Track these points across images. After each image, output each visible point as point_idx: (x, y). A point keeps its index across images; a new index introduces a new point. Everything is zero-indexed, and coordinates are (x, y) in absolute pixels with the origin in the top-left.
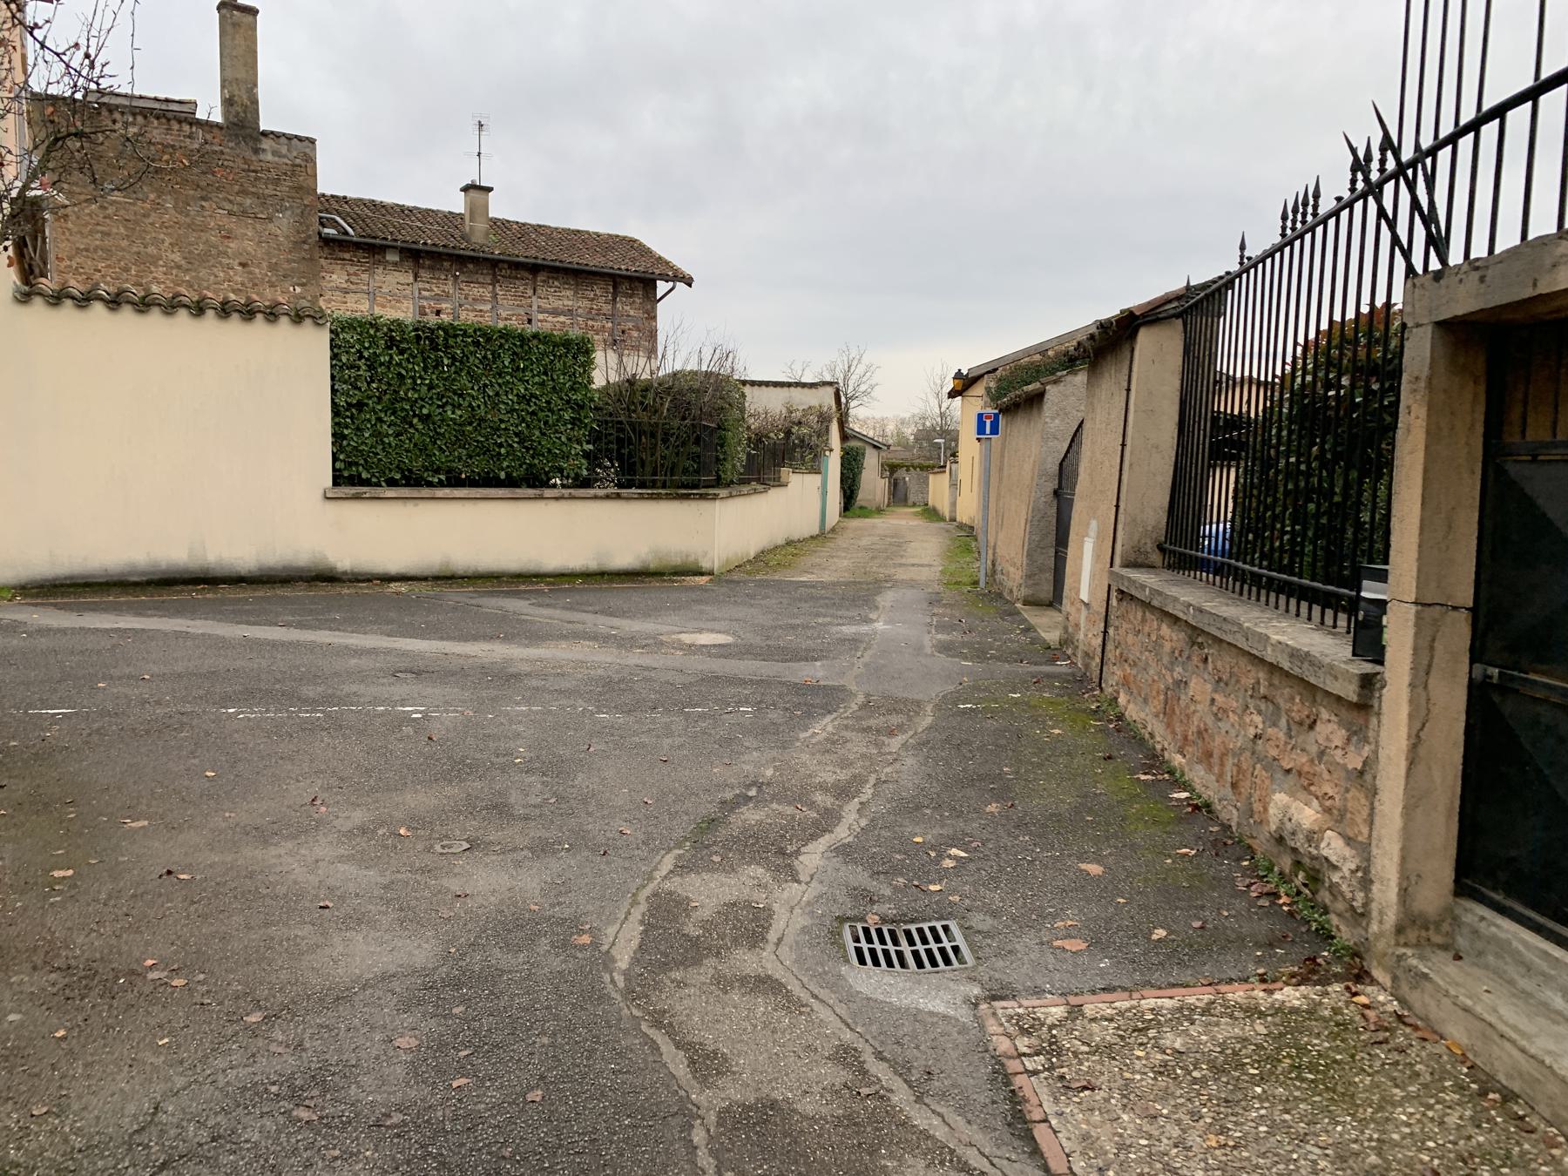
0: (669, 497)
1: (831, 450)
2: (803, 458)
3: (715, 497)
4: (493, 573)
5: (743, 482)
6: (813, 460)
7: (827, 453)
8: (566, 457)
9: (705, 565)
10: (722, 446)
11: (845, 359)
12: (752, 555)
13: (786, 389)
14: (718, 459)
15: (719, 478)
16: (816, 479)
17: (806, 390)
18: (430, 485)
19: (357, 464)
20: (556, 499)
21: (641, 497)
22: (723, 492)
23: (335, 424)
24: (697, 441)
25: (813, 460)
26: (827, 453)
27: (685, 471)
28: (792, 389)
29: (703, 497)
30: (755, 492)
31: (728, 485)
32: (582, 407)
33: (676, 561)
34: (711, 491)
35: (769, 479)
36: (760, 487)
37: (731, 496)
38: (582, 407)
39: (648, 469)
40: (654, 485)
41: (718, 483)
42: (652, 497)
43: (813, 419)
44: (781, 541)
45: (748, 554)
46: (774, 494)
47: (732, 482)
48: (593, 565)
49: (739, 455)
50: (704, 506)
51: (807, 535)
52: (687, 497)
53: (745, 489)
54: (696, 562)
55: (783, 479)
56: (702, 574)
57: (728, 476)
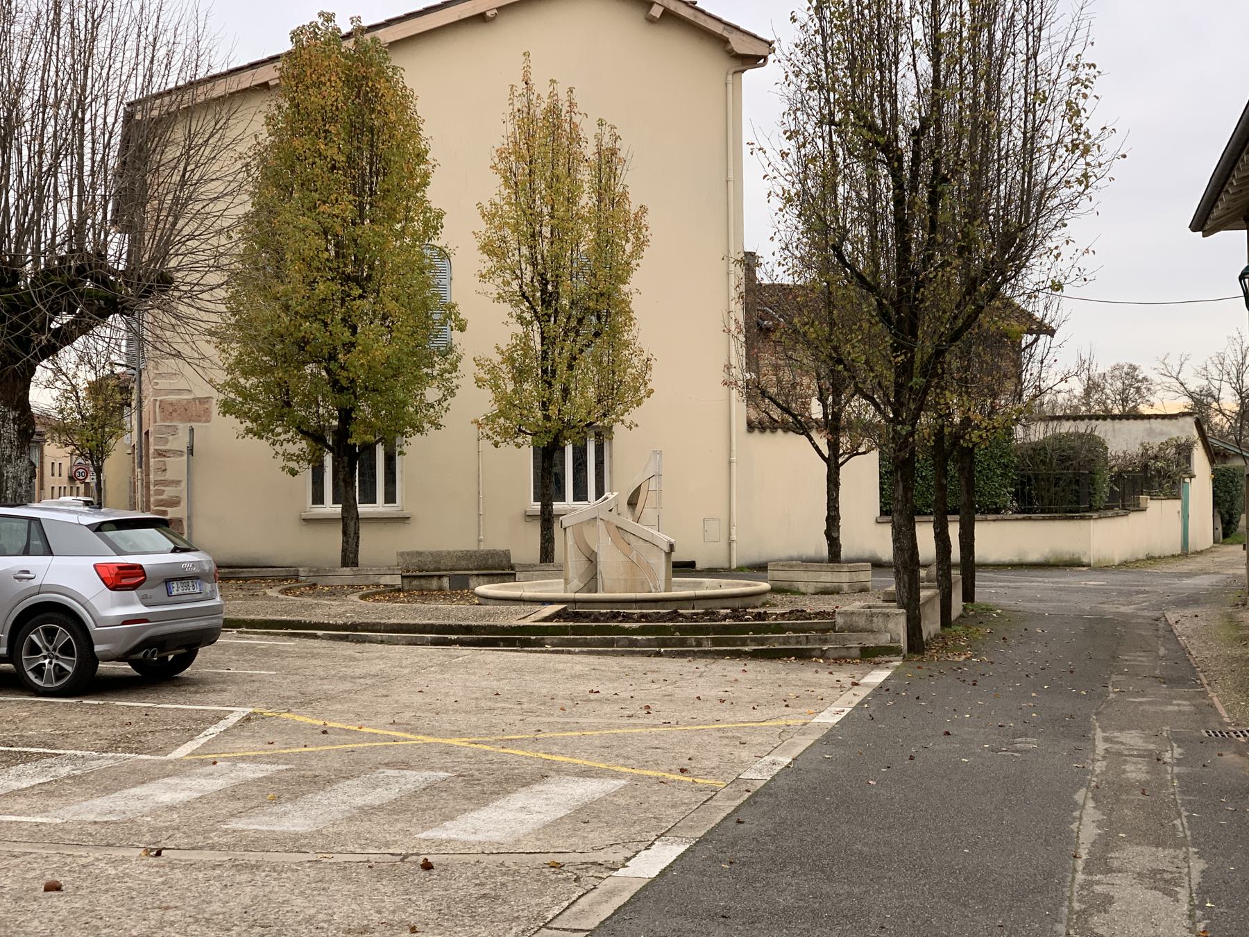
0: (1061, 519)
1: (1192, 477)
2: (1160, 485)
3: (1090, 518)
4: (1206, 452)
5: (1107, 508)
6: (1172, 488)
7: (1187, 480)
8: (998, 496)
9: (1085, 560)
10: (1093, 485)
11: (1238, 348)
12: (1117, 562)
13: (1146, 421)
14: (1090, 493)
15: (1091, 506)
16: (1177, 504)
17: (1166, 421)
18: (926, 514)
19: (889, 504)
20: (994, 520)
21: (1044, 519)
22: (1095, 515)
23: (881, 483)
24: (1077, 482)
25: (1172, 488)
26: (1187, 480)
27: (1070, 502)
28: (1152, 421)
29: (1082, 518)
30: (1117, 515)
31: (1097, 511)
32: (1007, 466)
33: (1067, 557)
34: (1088, 514)
35: (1130, 506)
36: (1121, 512)
37: (1100, 518)
38: (1007, 466)
39: (1046, 501)
40: (1050, 511)
41: (1091, 509)
42: (1051, 519)
43: (1171, 452)
44: (1141, 556)
45: (1113, 561)
46: (1134, 517)
47: (1100, 509)
48: (1016, 559)
49: (1105, 488)
50: (1083, 523)
51: (1168, 553)
52: (1072, 518)
53: (1110, 513)
54: (1079, 559)
55: (1142, 505)
56: (1083, 566)
57: (1096, 505)
